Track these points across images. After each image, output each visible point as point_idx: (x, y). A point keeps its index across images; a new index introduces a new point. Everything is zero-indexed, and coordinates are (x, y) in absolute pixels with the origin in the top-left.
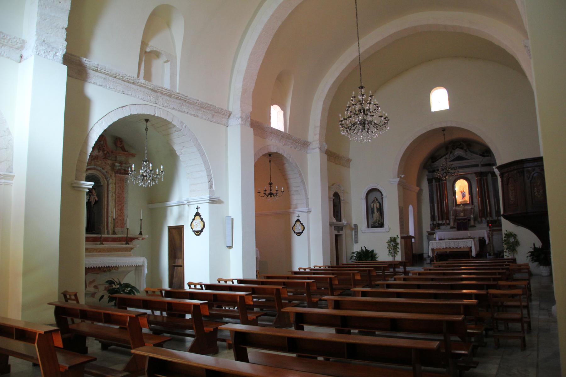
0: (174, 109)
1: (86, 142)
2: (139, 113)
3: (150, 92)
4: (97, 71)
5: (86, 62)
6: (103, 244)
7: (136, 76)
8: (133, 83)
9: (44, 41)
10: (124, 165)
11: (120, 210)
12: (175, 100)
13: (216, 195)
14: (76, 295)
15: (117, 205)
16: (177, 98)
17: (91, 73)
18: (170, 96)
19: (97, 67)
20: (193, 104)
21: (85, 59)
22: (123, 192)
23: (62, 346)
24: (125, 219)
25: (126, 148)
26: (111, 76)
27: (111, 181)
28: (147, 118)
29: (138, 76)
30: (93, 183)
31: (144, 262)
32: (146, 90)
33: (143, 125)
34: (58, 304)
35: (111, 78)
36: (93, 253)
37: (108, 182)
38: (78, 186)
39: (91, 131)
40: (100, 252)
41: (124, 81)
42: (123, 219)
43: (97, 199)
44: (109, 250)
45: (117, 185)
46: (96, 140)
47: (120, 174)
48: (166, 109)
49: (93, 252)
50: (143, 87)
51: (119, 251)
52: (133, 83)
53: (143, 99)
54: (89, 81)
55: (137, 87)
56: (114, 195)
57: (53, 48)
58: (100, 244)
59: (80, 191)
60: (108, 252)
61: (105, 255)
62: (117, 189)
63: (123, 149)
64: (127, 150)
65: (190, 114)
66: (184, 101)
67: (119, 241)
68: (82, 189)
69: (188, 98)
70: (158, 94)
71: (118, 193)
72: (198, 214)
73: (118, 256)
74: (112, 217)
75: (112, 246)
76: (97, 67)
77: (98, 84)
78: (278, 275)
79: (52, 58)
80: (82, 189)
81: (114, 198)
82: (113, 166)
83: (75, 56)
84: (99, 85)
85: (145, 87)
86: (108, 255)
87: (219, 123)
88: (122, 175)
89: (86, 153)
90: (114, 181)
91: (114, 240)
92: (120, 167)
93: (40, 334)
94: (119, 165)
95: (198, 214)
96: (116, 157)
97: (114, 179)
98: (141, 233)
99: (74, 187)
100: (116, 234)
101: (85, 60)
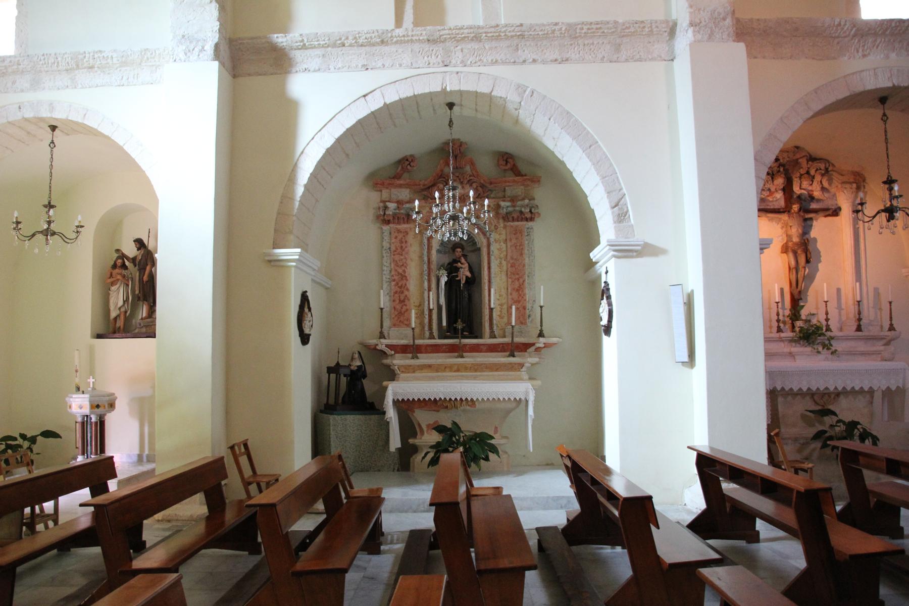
0: (495, 62)
1: (291, 179)
2: (403, 95)
3: (426, 47)
4: (304, 47)
5: (280, 40)
6: (462, 357)
7: (391, 25)
8: (382, 42)
9: (183, 36)
10: (519, 203)
11: (518, 290)
12: (494, 44)
13: (641, 235)
14: (246, 445)
15: (510, 280)
16: (498, 38)
17: (298, 55)
18: (477, 38)
19: (303, 41)
20: (546, 36)
21: (276, 35)
22: (522, 254)
24: (529, 306)
25: (523, 168)
26: (334, 45)
27: (494, 236)
29: (399, 22)
30: (299, 250)
31: (527, 393)
32: (416, 47)
34: (706, 451)
35: (334, 51)
36: (444, 374)
37: (488, 239)
38: (276, 258)
39: (302, 158)
40: (458, 370)
41: (362, 45)
42: (524, 308)
43: (469, 274)
44: (477, 368)
45: (509, 244)
46: (311, 171)
47: (513, 220)
48: (475, 69)
49: (444, 371)
50: (405, 42)
51: (497, 370)
52: (382, 42)
53: (411, 66)
54: (294, 70)
55: (393, 48)
56: (504, 263)
57: (198, 41)
58: (413, 358)
59: (283, 266)
60: (476, 371)
61: (467, 378)
62: (509, 251)
63: (516, 171)
64: (523, 173)
65: (544, 62)
66: (518, 39)
67: (501, 351)
68: (282, 264)
69: (523, 28)
70: (447, 44)
71: (512, 258)
73: (495, 379)
75: (479, 359)
76: (303, 41)
77: (312, 69)
78: (256, 466)
79: (196, 57)
80: (282, 264)
81: (505, 268)
82: (496, 208)
83: (260, 38)
84: (315, 71)
85: (412, 41)
86: (475, 378)
87: (640, 60)
88: (516, 223)
89: (292, 199)
90: (504, 237)
91: (492, 348)
92: (510, 209)
93: (798, 492)
94: (509, 204)
96: (505, 191)
97: (504, 232)
98: (892, 328)
99: (270, 261)
100: (495, 337)
101: (279, 39)
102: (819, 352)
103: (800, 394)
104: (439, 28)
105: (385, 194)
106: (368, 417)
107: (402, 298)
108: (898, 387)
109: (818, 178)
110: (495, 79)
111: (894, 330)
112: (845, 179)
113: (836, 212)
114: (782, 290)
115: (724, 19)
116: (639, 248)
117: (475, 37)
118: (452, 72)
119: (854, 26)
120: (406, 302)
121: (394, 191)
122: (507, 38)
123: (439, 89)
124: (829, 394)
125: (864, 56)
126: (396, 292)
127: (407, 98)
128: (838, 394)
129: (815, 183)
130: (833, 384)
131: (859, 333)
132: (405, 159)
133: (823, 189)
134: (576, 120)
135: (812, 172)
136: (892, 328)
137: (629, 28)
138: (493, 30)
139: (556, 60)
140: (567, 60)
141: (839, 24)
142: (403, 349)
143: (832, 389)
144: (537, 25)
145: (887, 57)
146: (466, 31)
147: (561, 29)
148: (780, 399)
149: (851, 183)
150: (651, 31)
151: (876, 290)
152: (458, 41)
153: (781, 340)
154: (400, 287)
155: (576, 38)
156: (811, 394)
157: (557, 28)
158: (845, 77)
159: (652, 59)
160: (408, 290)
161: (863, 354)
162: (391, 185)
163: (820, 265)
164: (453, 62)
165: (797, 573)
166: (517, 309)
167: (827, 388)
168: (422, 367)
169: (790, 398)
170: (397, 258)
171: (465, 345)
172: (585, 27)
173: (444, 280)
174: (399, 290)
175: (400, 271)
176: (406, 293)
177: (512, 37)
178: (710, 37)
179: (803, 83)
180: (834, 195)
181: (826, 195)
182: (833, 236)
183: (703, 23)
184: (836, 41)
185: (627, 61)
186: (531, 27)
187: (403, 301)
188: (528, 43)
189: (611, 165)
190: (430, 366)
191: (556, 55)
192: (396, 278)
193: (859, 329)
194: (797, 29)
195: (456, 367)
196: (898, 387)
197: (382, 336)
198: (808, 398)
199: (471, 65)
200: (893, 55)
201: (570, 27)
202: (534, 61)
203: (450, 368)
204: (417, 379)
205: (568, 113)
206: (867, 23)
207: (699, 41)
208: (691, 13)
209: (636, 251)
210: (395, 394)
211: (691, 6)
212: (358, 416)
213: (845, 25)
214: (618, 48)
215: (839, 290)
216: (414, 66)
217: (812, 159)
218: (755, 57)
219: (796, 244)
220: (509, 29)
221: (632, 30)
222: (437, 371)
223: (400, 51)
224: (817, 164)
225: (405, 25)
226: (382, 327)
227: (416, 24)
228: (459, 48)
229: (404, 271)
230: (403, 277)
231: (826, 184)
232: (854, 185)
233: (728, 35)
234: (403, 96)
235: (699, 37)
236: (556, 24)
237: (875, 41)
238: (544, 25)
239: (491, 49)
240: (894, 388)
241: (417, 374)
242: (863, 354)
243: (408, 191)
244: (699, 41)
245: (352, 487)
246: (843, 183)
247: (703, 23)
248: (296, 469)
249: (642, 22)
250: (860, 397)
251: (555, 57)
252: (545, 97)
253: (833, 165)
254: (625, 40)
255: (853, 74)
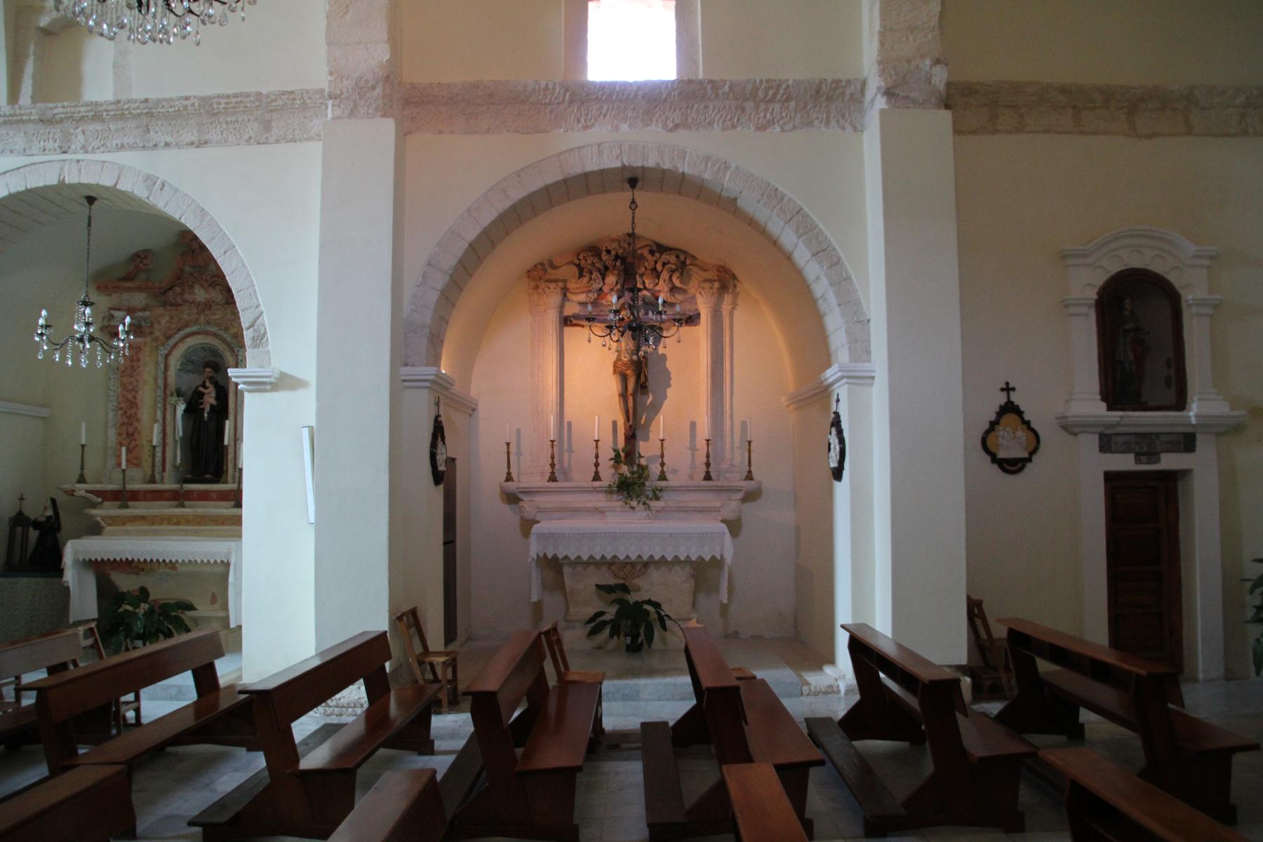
0: (121, 147)
3: (42, 129)
6: (183, 506)
12: (120, 124)
16: (120, 117)
23: (1083, 711)
28: (628, 175)
33: (84, 209)
40: (178, 524)
44: (201, 520)
48: (98, 156)
51: (223, 524)
53: (24, 152)
60: (199, 524)
65: (179, 146)
72: (1010, 408)
74: (151, 441)
85: (23, 122)
86: (197, 533)
95: (1010, 408)
102: (632, 508)
103: (591, 562)
104: (50, 105)
105: (115, 299)
106: (50, 580)
107: (131, 431)
108: (713, 558)
109: (665, 275)
110: (121, 168)
111: (752, 479)
112: (708, 275)
113: (691, 319)
114: (615, 423)
115: (373, 88)
116: (273, 380)
117: (95, 115)
118: (71, 161)
119: (567, 90)
120: (136, 436)
121: (126, 296)
122: (134, 117)
123: (55, 182)
124: (633, 564)
125: (585, 128)
126: (123, 424)
127: (19, 193)
128: (646, 565)
129: (661, 282)
130: (630, 551)
131: (597, 484)
132: (136, 256)
133: (673, 289)
134: (212, 219)
135: (659, 267)
136: (749, 477)
137: (276, 100)
138: (113, 107)
139: (192, 143)
140: (206, 142)
141: (547, 88)
142: (106, 496)
143: (622, 557)
144: (165, 100)
145: (616, 128)
146: (82, 109)
147: (193, 105)
148: (566, 570)
149: (711, 281)
150: (304, 103)
151: (744, 424)
152: (78, 121)
153: (595, 490)
154: (129, 417)
155: (216, 114)
156: (611, 564)
157: (189, 103)
158: (558, 155)
159: (307, 139)
160: (138, 420)
161: (701, 511)
162: (116, 289)
163: (669, 391)
164: (73, 147)
165: (357, 796)
166: (128, 450)
167: (615, 557)
168: (188, 521)
169: (579, 568)
170: (125, 380)
171: (192, 492)
172: (223, 101)
173: (181, 408)
174: (126, 420)
175: (130, 396)
176: (136, 424)
177: (139, 115)
178: (353, 113)
179: (485, 169)
180: (694, 297)
181: (679, 297)
182: (685, 354)
183: (346, 94)
184: (549, 109)
185: (277, 141)
186: (158, 101)
187: (132, 435)
188: (159, 123)
189: (249, 275)
190: (143, 518)
191: (194, 138)
192: (124, 405)
193: (708, 477)
194: (491, 95)
195: (174, 520)
196: (713, 558)
197: (82, 480)
198: (605, 569)
199: (93, 152)
200: (625, 127)
201: (205, 101)
202: (167, 145)
203: (169, 520)
204: (128, 533)
205: (203, 210)
206: (594, 84)
207: (339, 118)
208: (330, 82)
209: (271, 383)
210: (75, 552)
211: (331, 73)
212: (34, 580)
213: (554, 89)
214: (267, 126)
215: (519, 431)
216: (28, 152)
217: (661, 249)
218: (441, 132)
219: (625, 364)
220: (133, 106)
221: (280, 103)
222: (153, 524)
223: (11, 133)
224: (665, 257)
225: (21, 102)
226: (82, 468)
227: (35, 99)
228: (80, 129)
229: (135, 397)
230: (133, 404)
231: (677, 283)
232: (717, 285)
233: (376, 109)
234: (13, 190)
235: (338, 112)
236: (187, 98)
237: (601, 107)
238: (171, 99)
239: (117, 130)
240: (707, 559)
241: (129, 527)
242: (701, 511)
243: (144, 295)
244: (339, 118)
245: (567, 668)
246: (706, 281)
247: (346, 94)
248: (889, 634)
249: (292, 92)
250: (677, 568)
251: (193, 139)
252: (177, 190)
253: (694, 257)
254: (275, 116)
255: (570, 150)
